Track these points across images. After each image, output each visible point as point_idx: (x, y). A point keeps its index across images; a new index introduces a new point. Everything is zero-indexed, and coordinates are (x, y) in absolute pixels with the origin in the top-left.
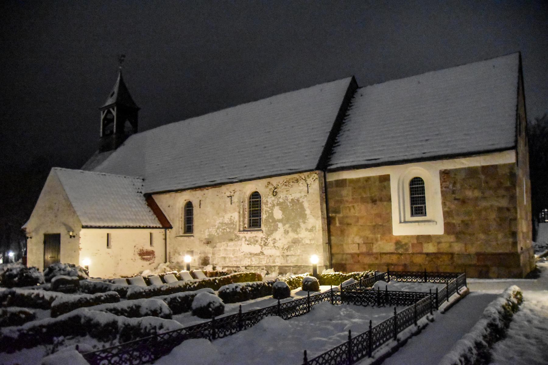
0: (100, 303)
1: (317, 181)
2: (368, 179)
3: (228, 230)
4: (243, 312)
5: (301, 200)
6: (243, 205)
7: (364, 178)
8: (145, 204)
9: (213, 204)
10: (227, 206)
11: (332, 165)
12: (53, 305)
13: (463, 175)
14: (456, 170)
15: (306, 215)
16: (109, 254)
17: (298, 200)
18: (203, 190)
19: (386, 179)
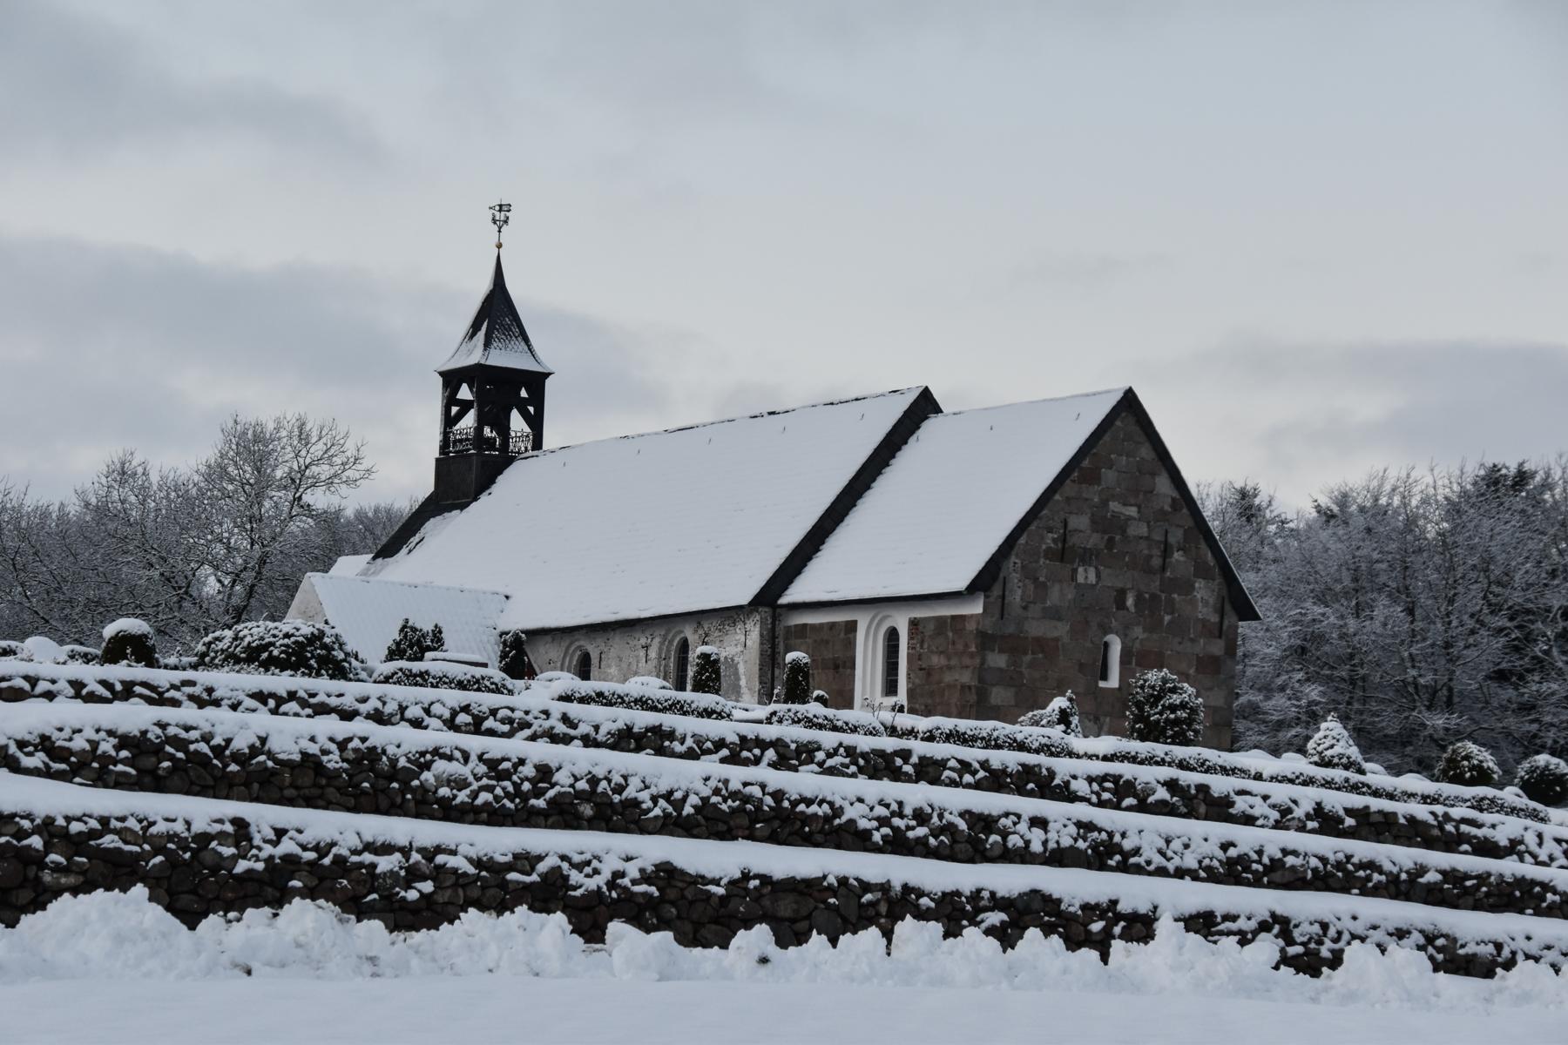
0: (446, 394)
1: (758, 626)
2: (832, 625)
3: (191, 541)
4: (873, 933)
5: (736, 659)
6: (666, 666)
7: (828, 623)
8: (1123, 835)
9: (621, 660)
10: (640, 665)
11: (44, 762)
12: (500, 767)
13: (932, 626)
14: (925, 619)
15: (740, 687)
16: (537, 975)
17: (733, 660)
18: (595, 638)
19: (852, 627)
